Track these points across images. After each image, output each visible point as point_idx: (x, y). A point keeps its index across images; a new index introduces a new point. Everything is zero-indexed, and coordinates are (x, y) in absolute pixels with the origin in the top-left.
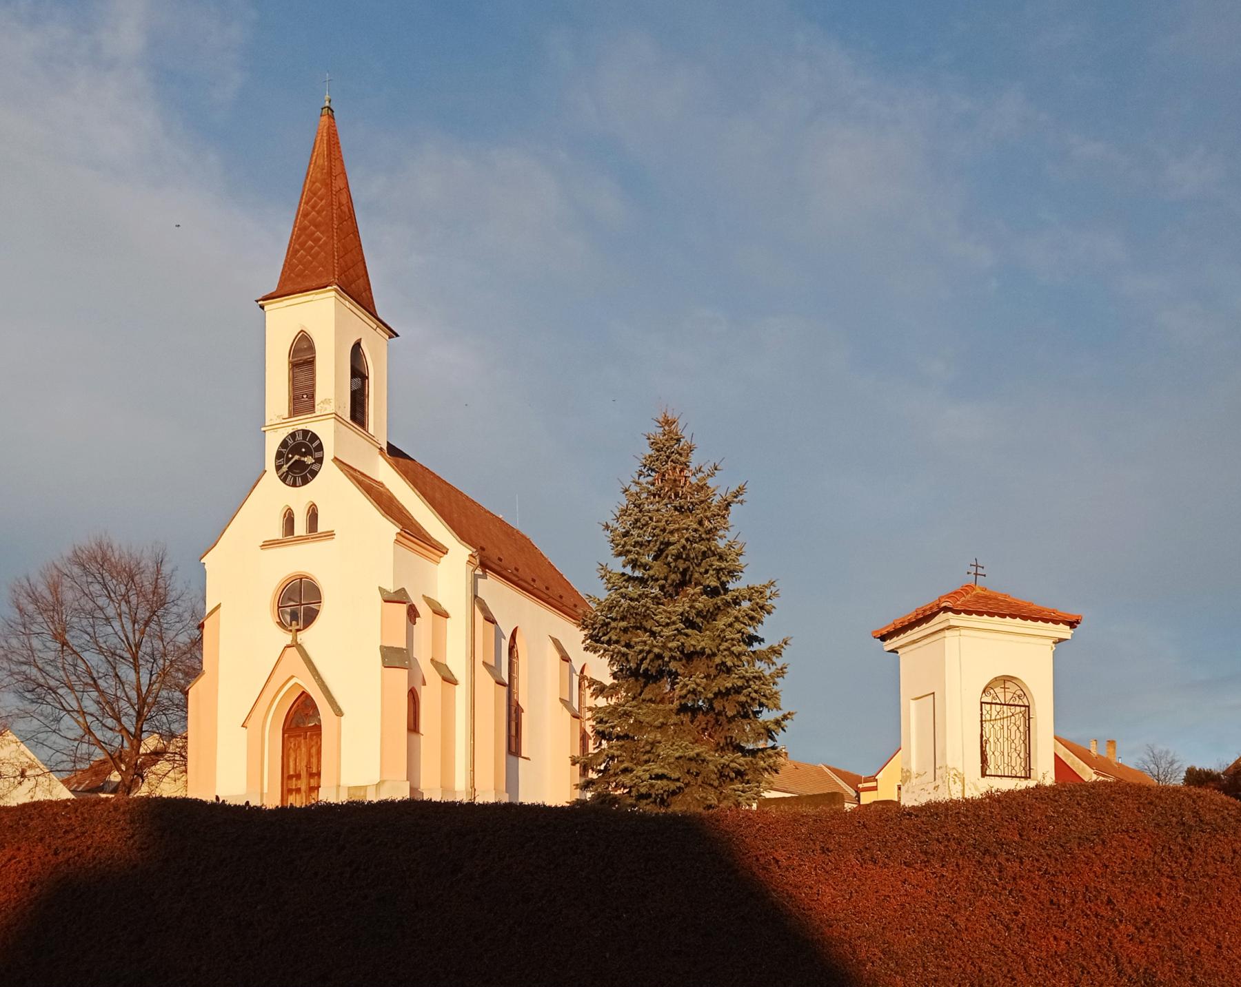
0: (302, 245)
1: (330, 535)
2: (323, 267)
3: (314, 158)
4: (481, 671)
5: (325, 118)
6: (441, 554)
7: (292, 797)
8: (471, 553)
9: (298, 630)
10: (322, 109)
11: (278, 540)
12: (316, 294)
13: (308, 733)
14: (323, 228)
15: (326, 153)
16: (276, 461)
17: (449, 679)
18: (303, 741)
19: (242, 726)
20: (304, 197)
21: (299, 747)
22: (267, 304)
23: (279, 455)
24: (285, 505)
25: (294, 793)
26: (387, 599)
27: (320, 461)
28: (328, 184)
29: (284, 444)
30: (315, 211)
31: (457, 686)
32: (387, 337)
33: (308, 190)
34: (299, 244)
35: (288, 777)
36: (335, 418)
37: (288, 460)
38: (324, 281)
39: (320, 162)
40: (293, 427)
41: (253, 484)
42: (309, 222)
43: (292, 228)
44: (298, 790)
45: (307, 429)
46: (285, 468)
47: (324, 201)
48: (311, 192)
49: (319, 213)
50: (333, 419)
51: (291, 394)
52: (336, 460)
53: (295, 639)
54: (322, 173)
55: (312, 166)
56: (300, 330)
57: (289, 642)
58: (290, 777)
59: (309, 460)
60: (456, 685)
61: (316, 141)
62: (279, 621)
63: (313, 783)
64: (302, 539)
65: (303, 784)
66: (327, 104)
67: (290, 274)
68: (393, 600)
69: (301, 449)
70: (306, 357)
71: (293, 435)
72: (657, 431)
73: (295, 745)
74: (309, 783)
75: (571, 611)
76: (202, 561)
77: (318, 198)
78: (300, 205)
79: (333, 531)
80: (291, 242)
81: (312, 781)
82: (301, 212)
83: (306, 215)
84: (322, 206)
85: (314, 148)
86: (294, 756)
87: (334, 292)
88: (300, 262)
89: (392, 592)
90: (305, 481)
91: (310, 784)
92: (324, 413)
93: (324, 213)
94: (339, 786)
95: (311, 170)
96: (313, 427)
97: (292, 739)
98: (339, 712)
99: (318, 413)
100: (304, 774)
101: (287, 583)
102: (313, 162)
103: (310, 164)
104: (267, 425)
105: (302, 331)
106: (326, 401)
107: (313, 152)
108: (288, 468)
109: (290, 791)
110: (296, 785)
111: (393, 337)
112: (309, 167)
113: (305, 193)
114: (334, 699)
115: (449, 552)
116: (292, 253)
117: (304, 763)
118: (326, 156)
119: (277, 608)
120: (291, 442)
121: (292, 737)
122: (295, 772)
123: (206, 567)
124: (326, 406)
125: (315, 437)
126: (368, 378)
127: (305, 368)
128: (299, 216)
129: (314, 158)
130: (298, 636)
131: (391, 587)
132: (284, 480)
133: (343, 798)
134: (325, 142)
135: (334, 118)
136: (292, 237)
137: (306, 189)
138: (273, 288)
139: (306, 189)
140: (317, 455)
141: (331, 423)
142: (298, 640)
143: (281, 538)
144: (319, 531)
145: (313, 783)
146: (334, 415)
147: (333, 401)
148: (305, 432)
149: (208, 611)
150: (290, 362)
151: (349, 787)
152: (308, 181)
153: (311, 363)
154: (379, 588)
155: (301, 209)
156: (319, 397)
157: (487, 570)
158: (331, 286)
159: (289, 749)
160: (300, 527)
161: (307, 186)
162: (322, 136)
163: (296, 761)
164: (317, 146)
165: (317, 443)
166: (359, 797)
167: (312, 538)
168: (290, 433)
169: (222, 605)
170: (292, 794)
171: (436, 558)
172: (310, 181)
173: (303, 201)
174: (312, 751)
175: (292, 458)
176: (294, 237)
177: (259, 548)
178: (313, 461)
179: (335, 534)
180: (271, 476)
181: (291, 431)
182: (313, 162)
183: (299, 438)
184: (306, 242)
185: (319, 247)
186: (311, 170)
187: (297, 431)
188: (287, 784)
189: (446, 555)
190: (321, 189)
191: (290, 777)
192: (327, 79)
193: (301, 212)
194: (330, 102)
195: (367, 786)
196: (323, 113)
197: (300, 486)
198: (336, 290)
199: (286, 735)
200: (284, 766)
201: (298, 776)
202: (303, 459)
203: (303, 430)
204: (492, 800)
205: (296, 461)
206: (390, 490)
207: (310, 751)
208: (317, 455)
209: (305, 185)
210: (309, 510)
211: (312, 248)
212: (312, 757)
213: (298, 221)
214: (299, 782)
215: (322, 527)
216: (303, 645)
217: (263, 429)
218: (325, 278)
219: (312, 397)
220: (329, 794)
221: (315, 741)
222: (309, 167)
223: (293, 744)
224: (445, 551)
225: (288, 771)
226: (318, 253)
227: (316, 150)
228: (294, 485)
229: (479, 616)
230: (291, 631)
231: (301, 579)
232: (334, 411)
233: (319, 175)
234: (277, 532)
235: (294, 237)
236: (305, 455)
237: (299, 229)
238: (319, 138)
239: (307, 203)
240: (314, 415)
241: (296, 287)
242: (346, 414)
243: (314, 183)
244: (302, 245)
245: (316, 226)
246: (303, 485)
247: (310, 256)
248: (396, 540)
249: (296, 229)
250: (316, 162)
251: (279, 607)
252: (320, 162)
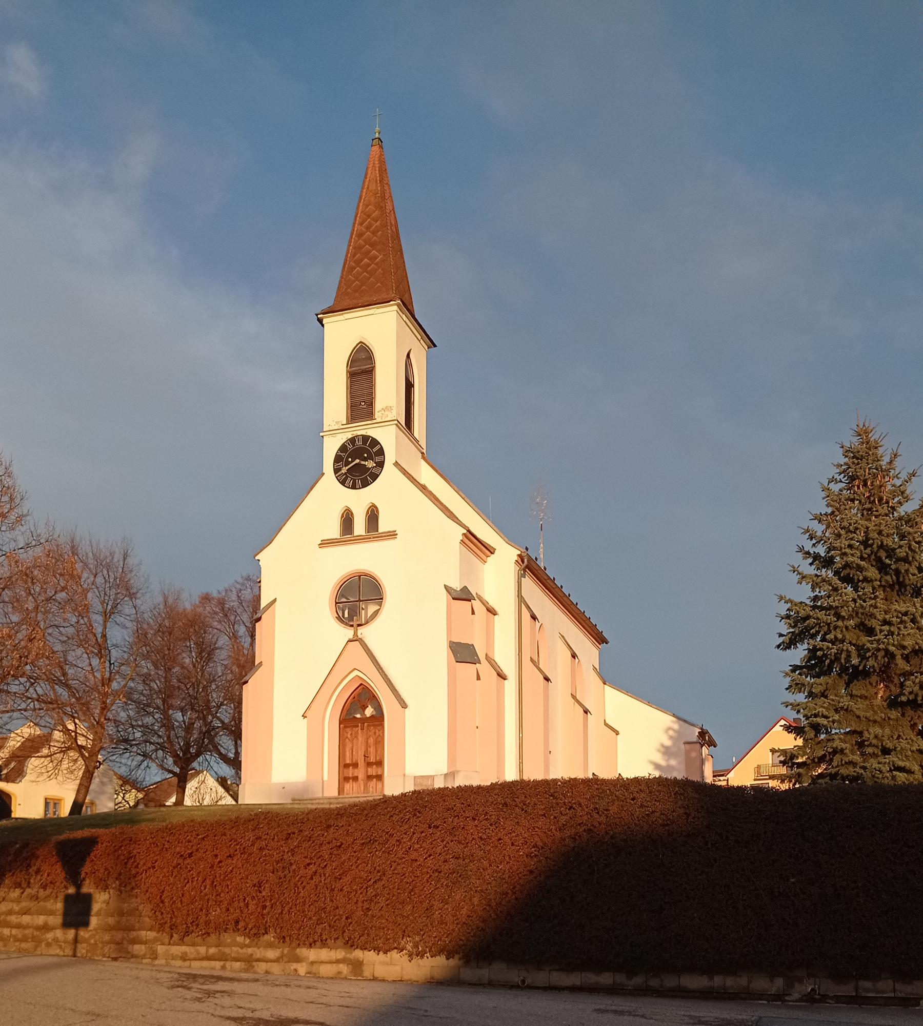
1: (392, 535)
2: (381, 283)
3: (367, 183)
4: (527, 665)
5: (376, 148)
6: (488, 553)
8: (519, 553)
9: (359, 625)
10: (373, 140)
11: (336, 539)
12: (378, 308)
13: (366, 724)
14: (379, 247)
15: (378, 179)
17: (502, 676)
19: (304, 716)
20: (358, 218)
21: (356, 737)
23: (338, 459)
25: (351, 781)
26: (456, 597)
27: (381, 465)
28: (382, 207)
29: (343, 448)
30: (370, 232)
31: (506, 681)
32: (426, 347)
33: (362, 212)
34: (355, 262)
35: (346, 768)
36: (396, 425)
38: (384, 296)
39: (373, 187)
41: (311, 485)
42: (365, 241)
44: (355, 779)
45: (368, 434)
46: (344, 470)
47: (378, 223)
48: (365, 214)
49: (374, 233)
51: (349, 401)
52: (396, 464)
53: (355, 634)
54: (376, 197)
55: (365, 190)
57: (351, 637)
58: (347, 766)
59: (370, 464)
60: (505, 679)
63: (372, 771)
64: (360, 539)
65: (360, 772)
66: (377, 135)
67: (346, 289)
69: (364, 454)
70: (365, 367)
71: (352, 440)
72: (852, 441)
73: (351, 734)
74: (367, 771)
77: (373, 219)
78: (354, 226)
79: (395, 531)
81: (369, 769)
82: (355, 232)
83: (360, 235)
86: (351, 745)
89: (458, 590)
90: (365, 484)
92: (386, 420)
94: (404, 775)
95: (364, 194)
96: (374, 433)
97: (348, 730)
98: (404, 705)
99: (378, 420)
100: (361, 763)
101: (346, 580)
103: (363, 188)
104: (324, 430)
105: (361, 342)
106: (388, 409)
107: (366, 178)
109: (347, 779)
110: (353, 774)
111: (431, 347)
112: (362, 191)
115: (496, 551)
116: (347, 270)
117: (361, 753)
118: (378, 182)
119: (334, 603)
122: (352, 761)
123: (260, 563)
124: (387, 413)
125: (375, 442)
126: (413, 386)
127: (364, 377)
128: (354, 236)
131: (457, 585)
132: (343, 483)
133: (409, 788)
134: (377, 169)
136: (347, 256)
137: (360, 212)
138: (329, 303)
139: (360, 212)
140: (378, 459)
141: (393, 429)
142: (359, 634)
143: (339, 537)
144: (380, 530)
145: (372, 771)
146: (396, 422)
147: (394, 409)
148: (365, 438)
149: (262, 606)
150: (347, 371)
151: (415, 777)
152: (361, 204)
153: (369, 372)
155: (356, 229)
156: (379, 404)
159: (345, 740)
160: (360, 527)
161: (361, 208)
162: (374, 164)
163: (352, 751)
164: (369, 172)
165: (378, 447)
167: (374, 538)
168: (349, 438)
170: (348, 782)
171: (484, 557)
173: (357, 222)
174: (369, 742)
175: (352, 461)
178: (375, 465)
179: (397, 534)
181: (350, 436)
183: (359, 443)
184: (362, 260)
185: (376, 264)
186: (364, 194)
187: (357, 436)
190: (375, 211)
191: (347, 766)
192: (378, 114)
193: (355, 232)
195: (434, 776)
196: (374, 144)
197: (360, 488)
198: (398, 305)
199: (341, 725)
200: (341, 755)
201: (355, 765)
202: (363, 463)
203: (361, 435)
204: (442, 786)
205: (356, 464)
207: (367, 742)
208: (378, 459)
209: (358, 208)
210: (368, 511)
211: (369, 265)
212: (370, 747)
213: (353, 240)
215: (383, 527)
216: (364, 640)
217: (321, 434)
219: (371, 404)
220: (393, 787)
222: (362, 191)
223: (349, 734)
224: (492, 551)
225: (344, 760)
226: (375, 270)
227: (368, 176)
228: (354, 487)
229: (526, 615)
230: (352, 626)
231: (360, 576)
232: (395, 418)
233: (372, 199)
234: (334, 531)
235: (349, 255)
236: (365, 459)
237: (354, 248)
239: (361, 224)
240: (374, 421)
241: (355, 301)
243: (367, 206)
244: (358, 262)
245: (371, 245)
246: (363, 487)
247: (367, 272)
248: (461, 540)
250: (368, 187)
251: (336, 603)
252: (373, 187)
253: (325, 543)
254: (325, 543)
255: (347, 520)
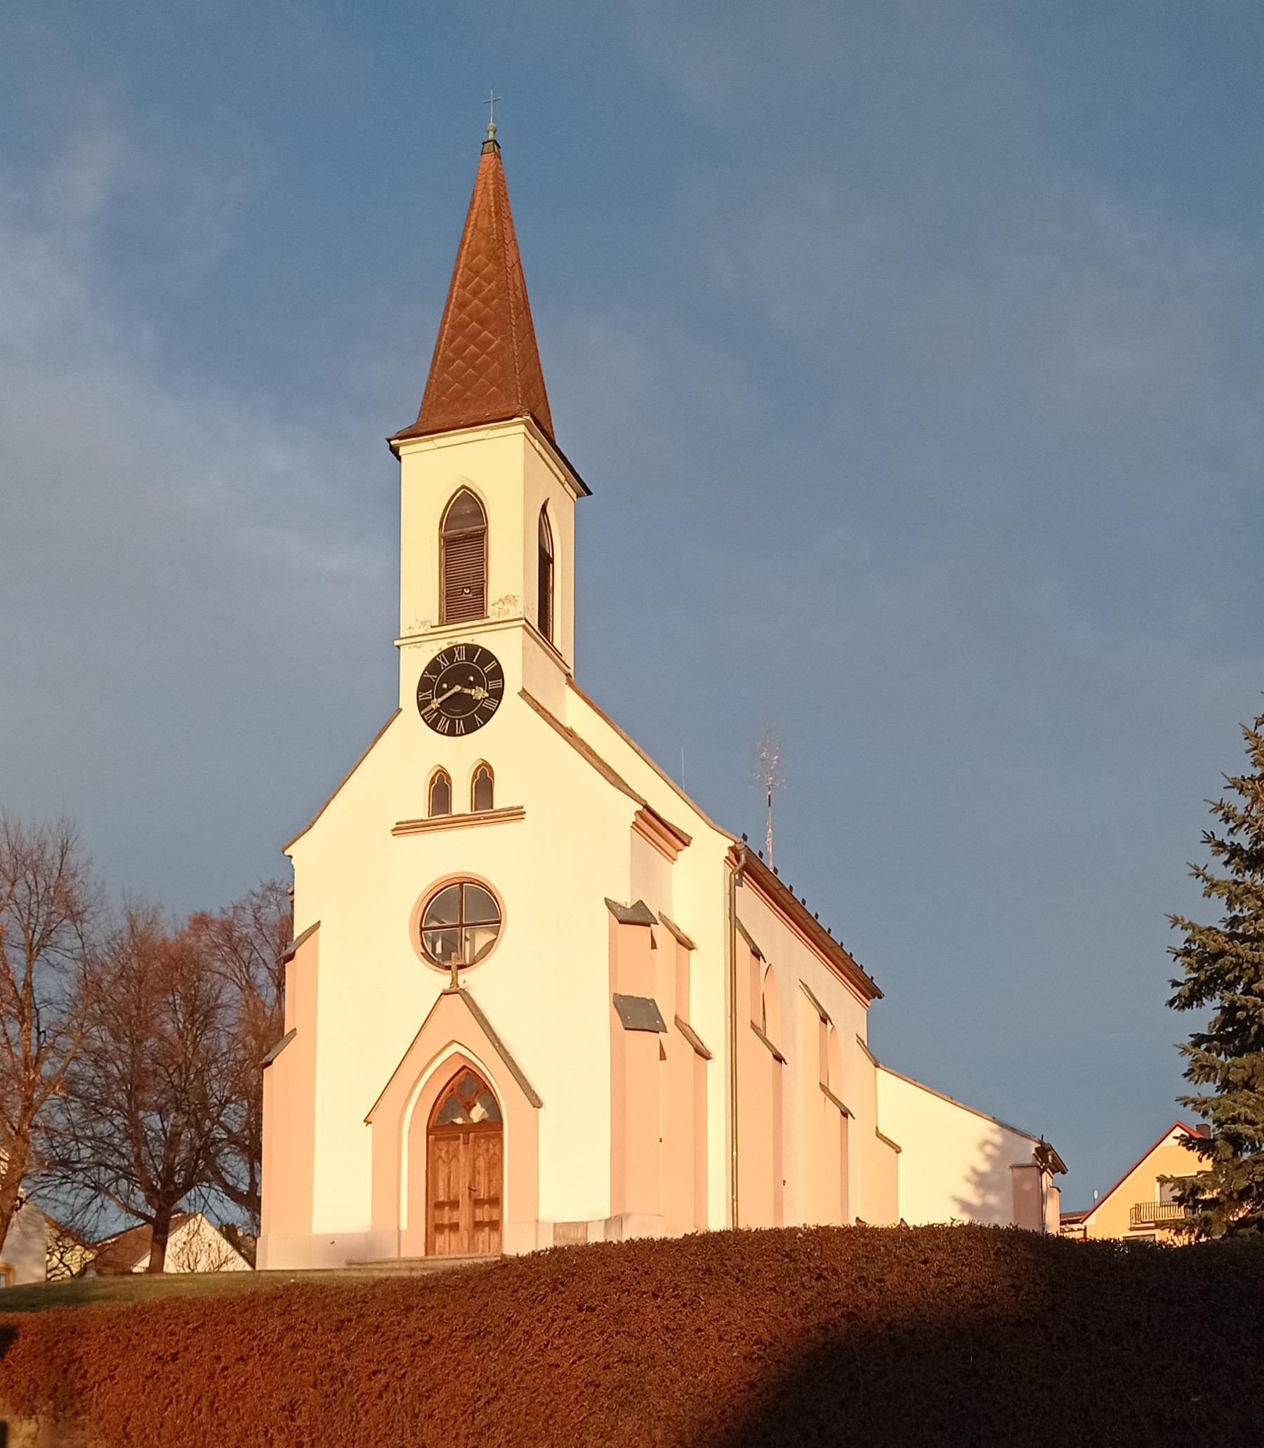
0: (459, 351)
1: (516, 813)
2: (498, 386)
3: (473, 217)
5: (489, 158)
6: (680, 845)
7: (442, 1237)
8: (732, 844)
9: (461, 967)
10: (484, 143)
11: (422, 820)
12: (492, 429)
13: (471, 1135)
14: (493, 326)
15: (493, 209)
16: (418, 695)
18: (461, 1146)
19: (367, 1122)
20: (458, 276)
21: (456, 1156)
22: (404, 445)
23: (424, 685)
24: (435, 764)
27: (497, 694)
28: (499, 258)
29: (433, 667)
30: (479, 299)
32: (574, 495)
33: (465, 266)
34: (453, 350)
36: (524, 626)
37: (443, 692)
38: (502, 408)
39: (484, 223)
40: (449, 640)
42: (469, 315)
43: (439, 325)
44: (454, 1227)
45: (475, 643)
46: (435, 704)
47: (493, 284)
48: (470, 269)
49: (486, 301)
50: (521, 628)
52: (524, 694)
53: (454, 981)
55: (470, 229)
56: (460, 485)
58: (439, 1206)
59: (479, 693)
61: (474, 192)
62: (424, 951)
63: (483, 1214)
65: (463, 1217)
66: (491, 136)
68: (632, 919)
69: (470, 676)
71: (449, 653)
73: (447, 1152)
74: (474, 1215)
75: (813, 934)
76: (287, 853)
77: (484, 278)
78: (452, 290)
79: (522, 807)
80: (438, 347)
81: (478, 1212)
83: (462, 305)
84: (490, 290)
85: (472, 203)
87: (523, 426)
88: (456, 379)
89: (629, 906)
90: (471, 728)
91: (474, 1218)
93: (496, 301)
94: (537, 1221)
95: (469, 235)
96: (486, 640)
98: (537, 1103)
99: (493, 619)
101: (438, 890)
102: (472, 223)
103: (467, 226)
104: (402, 636)
105: (463, 487)
108: (430, 704)
109: (439, 1228)
111: (583, 495)
112: (465, 231)
113: (460, 271)
114: (526, 1080)
115: (692, 841)
116: (441, 364)
118: (493, 215)
119: (419, 929)
120: (445, 664)
121: (443, 1140)
122: (449, 1197)
123: (293, 862)
124: (507, 606)
125: (487, 657)
126: (552, 561)
127: (468, 545)
129: (473, 217)
130: (459, 977)
131: (626, 899)
132: (433, 725)
133: (546, 1242)
134: (491, 193)
135: (500, 158)
136: (439, 340)
137: (462, 266)
138: (410, 420)
139: (462, 266)
140: (492, 685)
145: (483, 1214)
146: (523, 622)
148: (471, 649)
150: (441, 536)
151: (555, 1225)
152: (464, 253)
153: (478, 538)
154: (606, 899)
155: (455, 295)
157: (745, 873)
158: (521, 416)
159: (437, 1161)
160: (461, 800)
161: (463, 259)
163: (449, 1180)
164: (478, 199)
165: (492, 665)
166: (573, 1239)
168: (444, 648)
169: (322, 924)
170: (442, 1233)
171: (672, 851)
172: (468, 253)
173: (457, 283)
175: (449, 689)
176: (444, 340)
177: (390, 834)
178: (487, 695)
180: (410, 719)
181: (445, 647)
182: (472, 223)
183: (461, 658)
185: (489, 354)
187: (456, 646)
188: (434, 1216)
189: (687, 847)
191: (439, 1206)
193: (453, 301)
194: (495, 132)
195: (587, 1223)
196: (486, 150)
197: (462, 734)
198: (527, 424)
201: (454, 1205)
202: (467, 691)
204: (601, 1240)
205: (455, 694)
206: (585, 741)
207: (474, 1165)
209: (458, 260)
210: (475, 773)
211: (477, 356)
213: (450, 313)
214: (455, 1213)
215: (501, 800)
216: (470, 992)
217: (397, 643)
218: (504, 404)
219: (480, 592)
221: (485, 1147)
222: (465, 231)
224: (686, 841)
225: (436, 1196)
226: (487, 365)
227: (476, 205)
228: (451, 733)
229: (743, 949)
230: (449, 968)
231: (462, 884)
232: (522, 616)
234: (419, 808)
235: (444, 340)
237: (452, 327)
238: (481, 187)
239: (463, 286)
240: (487, 621)
241: (455, 418)
242: (535, 624)
243: (475, 256)
244: (459, 351)
245: (481, 322)
249: (447, 326)
251: (422, 929)
252: (484, 223)
253: (403, 828)
254: (403, 828)
255: (441, 789)
